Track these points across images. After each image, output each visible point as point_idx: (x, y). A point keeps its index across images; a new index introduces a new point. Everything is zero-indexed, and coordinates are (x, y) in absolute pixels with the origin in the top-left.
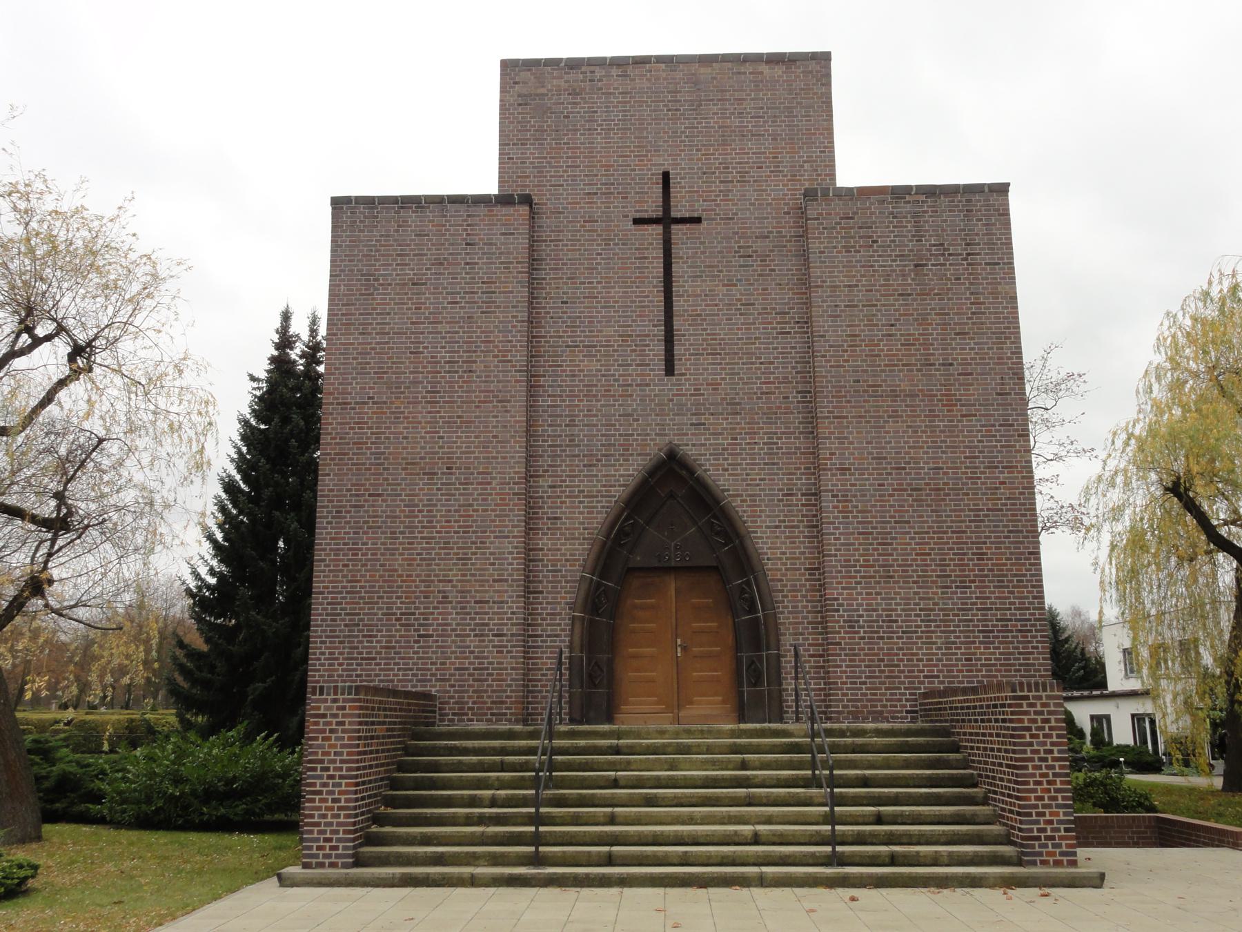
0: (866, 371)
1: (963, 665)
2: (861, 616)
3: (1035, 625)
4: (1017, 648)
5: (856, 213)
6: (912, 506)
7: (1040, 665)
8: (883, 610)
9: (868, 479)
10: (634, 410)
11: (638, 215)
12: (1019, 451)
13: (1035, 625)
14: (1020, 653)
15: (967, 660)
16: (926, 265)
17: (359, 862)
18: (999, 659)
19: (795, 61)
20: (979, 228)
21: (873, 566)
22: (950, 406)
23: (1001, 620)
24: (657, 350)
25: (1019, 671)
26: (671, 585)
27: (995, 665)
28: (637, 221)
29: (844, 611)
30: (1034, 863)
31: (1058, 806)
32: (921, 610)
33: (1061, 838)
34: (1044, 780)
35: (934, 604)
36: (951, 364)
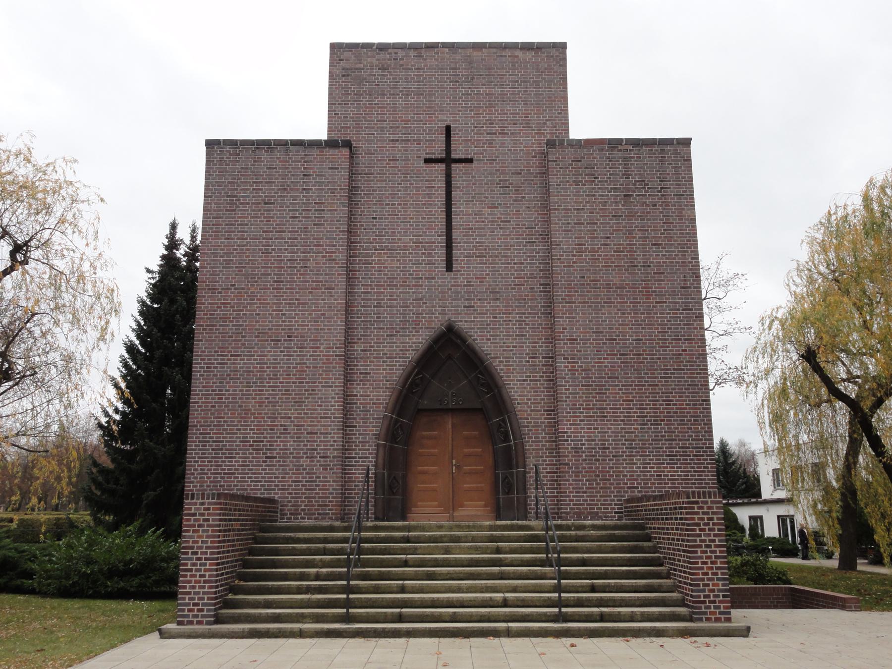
0: (589, 270)
2: (584, 444)
4: (694, 468)
6: (620, 366)
7: (709, 480)
10: (423, 296)
11: (428, 157)
14: (695, 471)
17: (218, 620)
18: (681, 476)
20: (670, 170)
23: (682, 448)
24: (440, 254)
26: (449, 422)
28: (427, 161)
30: (701, 620)
31: (718, 579)
33: (720, 602)
34: (709, 561)
36: (649, 266)
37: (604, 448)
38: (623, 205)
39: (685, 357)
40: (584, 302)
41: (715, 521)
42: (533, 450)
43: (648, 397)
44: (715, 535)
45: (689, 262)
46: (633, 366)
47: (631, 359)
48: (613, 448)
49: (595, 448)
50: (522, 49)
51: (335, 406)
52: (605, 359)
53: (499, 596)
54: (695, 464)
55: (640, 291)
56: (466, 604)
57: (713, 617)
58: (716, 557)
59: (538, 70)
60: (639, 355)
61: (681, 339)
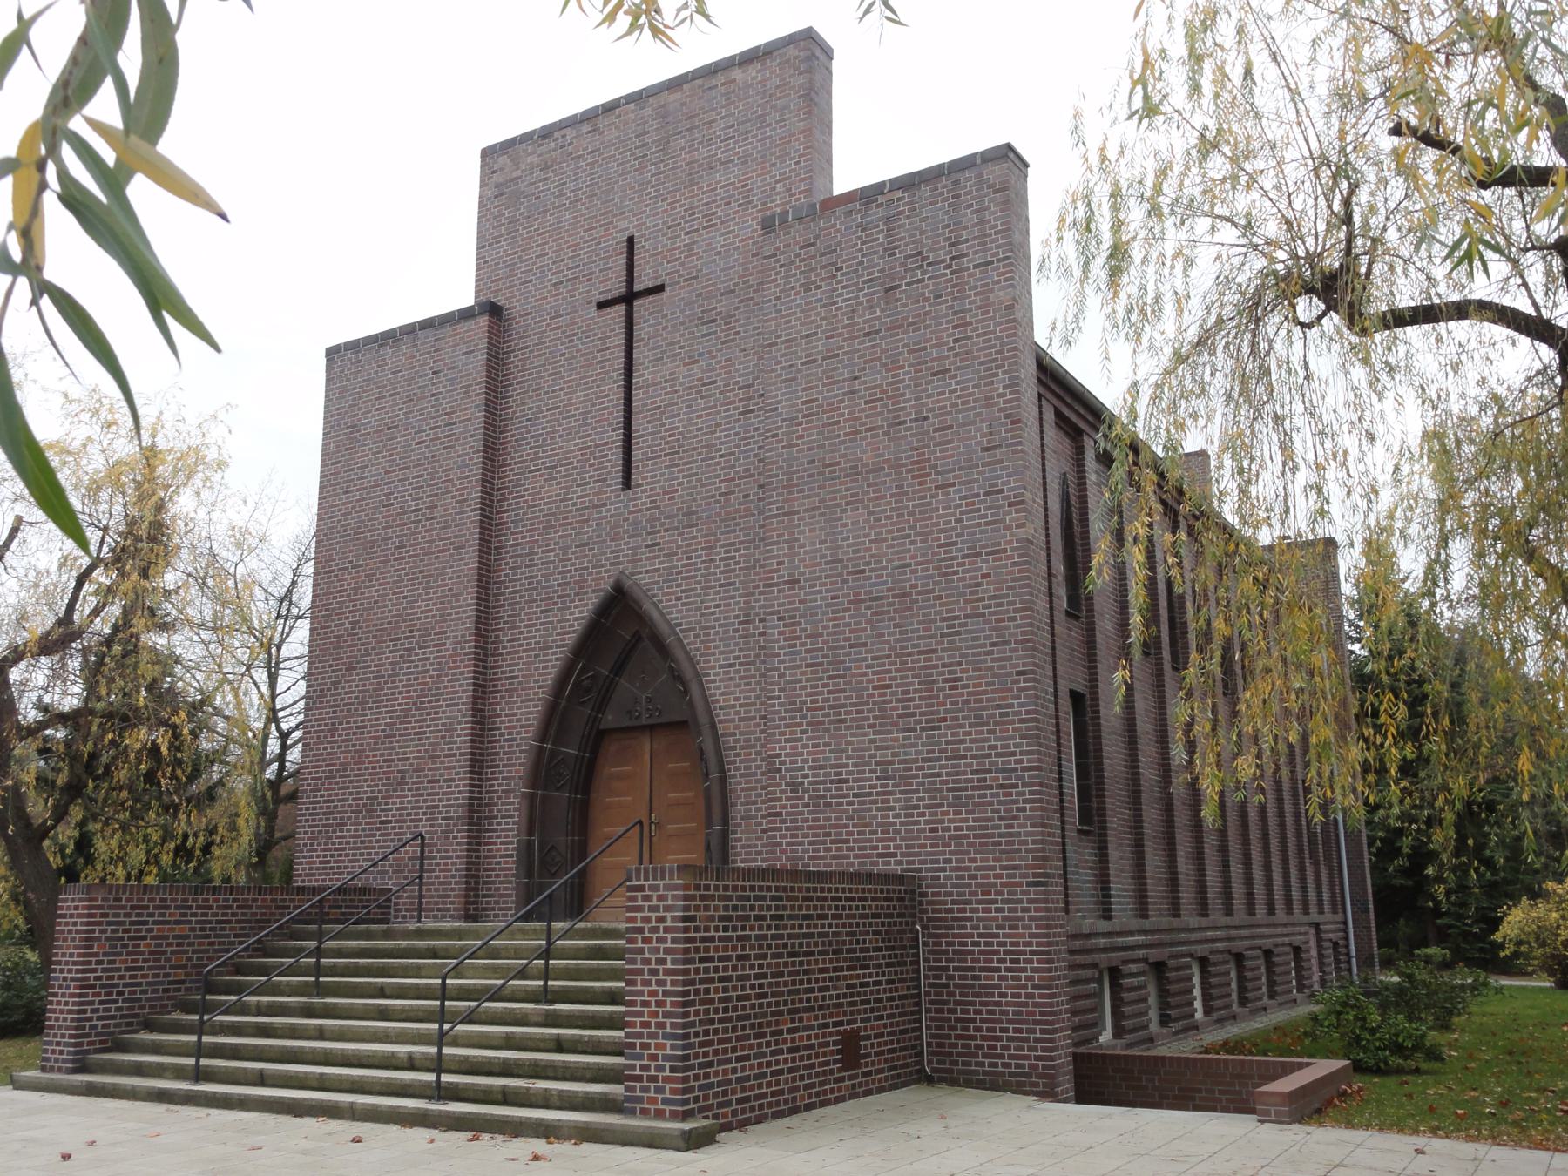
0: (822, 446)
1: (926, 838)
2: (806, 776)
3: (1022, 777)
4: (998, 811)
6: (871, 622)
7: (1027, 834)
8: (832, 767)
9: (820, 592)
10: (590, 538)
11: (602, 298)
12: (1009, 528)
13: (1022, 777)
14: (1001, 819)
15: (931, 830)
16: (899, 286)
17: (83, 1068)
18: (973, 828)
19: (770, 53)
20: (968, 218)
21: (822, 708)
22: (922, 477)
23: (977, 772)
24: (617, 457)
25: (999, 843)
26: (645, 745)
27: (967, 836)
29: (787, 770)
30: (632, 1112)
31: (665, 1036)
32: (877, 763)
33: (666, 1079)
34: (653, 999)
35: (894, 754)
36: (926, 418)
37: (840, 781)
38: (882, 310)
39: (988, 589)
40: (813, 509)
41: (669, 924)
42: (742, 790)
43: (918, 676)
44: (667, 951)
45: (999, 396)
46: (894, 619)
47: (890, 604)
48: (855, 780)
49: (824, 782)
50: (741, 64)
51: (462, 735)
52: (845, 610)
53: (403, 1049)
54: (999, 803)
55: (909, 471)
56: (365, 1062)
57: (653, 1108)
58: (665, 993)
60: (904, 595)
61: (980, 554)
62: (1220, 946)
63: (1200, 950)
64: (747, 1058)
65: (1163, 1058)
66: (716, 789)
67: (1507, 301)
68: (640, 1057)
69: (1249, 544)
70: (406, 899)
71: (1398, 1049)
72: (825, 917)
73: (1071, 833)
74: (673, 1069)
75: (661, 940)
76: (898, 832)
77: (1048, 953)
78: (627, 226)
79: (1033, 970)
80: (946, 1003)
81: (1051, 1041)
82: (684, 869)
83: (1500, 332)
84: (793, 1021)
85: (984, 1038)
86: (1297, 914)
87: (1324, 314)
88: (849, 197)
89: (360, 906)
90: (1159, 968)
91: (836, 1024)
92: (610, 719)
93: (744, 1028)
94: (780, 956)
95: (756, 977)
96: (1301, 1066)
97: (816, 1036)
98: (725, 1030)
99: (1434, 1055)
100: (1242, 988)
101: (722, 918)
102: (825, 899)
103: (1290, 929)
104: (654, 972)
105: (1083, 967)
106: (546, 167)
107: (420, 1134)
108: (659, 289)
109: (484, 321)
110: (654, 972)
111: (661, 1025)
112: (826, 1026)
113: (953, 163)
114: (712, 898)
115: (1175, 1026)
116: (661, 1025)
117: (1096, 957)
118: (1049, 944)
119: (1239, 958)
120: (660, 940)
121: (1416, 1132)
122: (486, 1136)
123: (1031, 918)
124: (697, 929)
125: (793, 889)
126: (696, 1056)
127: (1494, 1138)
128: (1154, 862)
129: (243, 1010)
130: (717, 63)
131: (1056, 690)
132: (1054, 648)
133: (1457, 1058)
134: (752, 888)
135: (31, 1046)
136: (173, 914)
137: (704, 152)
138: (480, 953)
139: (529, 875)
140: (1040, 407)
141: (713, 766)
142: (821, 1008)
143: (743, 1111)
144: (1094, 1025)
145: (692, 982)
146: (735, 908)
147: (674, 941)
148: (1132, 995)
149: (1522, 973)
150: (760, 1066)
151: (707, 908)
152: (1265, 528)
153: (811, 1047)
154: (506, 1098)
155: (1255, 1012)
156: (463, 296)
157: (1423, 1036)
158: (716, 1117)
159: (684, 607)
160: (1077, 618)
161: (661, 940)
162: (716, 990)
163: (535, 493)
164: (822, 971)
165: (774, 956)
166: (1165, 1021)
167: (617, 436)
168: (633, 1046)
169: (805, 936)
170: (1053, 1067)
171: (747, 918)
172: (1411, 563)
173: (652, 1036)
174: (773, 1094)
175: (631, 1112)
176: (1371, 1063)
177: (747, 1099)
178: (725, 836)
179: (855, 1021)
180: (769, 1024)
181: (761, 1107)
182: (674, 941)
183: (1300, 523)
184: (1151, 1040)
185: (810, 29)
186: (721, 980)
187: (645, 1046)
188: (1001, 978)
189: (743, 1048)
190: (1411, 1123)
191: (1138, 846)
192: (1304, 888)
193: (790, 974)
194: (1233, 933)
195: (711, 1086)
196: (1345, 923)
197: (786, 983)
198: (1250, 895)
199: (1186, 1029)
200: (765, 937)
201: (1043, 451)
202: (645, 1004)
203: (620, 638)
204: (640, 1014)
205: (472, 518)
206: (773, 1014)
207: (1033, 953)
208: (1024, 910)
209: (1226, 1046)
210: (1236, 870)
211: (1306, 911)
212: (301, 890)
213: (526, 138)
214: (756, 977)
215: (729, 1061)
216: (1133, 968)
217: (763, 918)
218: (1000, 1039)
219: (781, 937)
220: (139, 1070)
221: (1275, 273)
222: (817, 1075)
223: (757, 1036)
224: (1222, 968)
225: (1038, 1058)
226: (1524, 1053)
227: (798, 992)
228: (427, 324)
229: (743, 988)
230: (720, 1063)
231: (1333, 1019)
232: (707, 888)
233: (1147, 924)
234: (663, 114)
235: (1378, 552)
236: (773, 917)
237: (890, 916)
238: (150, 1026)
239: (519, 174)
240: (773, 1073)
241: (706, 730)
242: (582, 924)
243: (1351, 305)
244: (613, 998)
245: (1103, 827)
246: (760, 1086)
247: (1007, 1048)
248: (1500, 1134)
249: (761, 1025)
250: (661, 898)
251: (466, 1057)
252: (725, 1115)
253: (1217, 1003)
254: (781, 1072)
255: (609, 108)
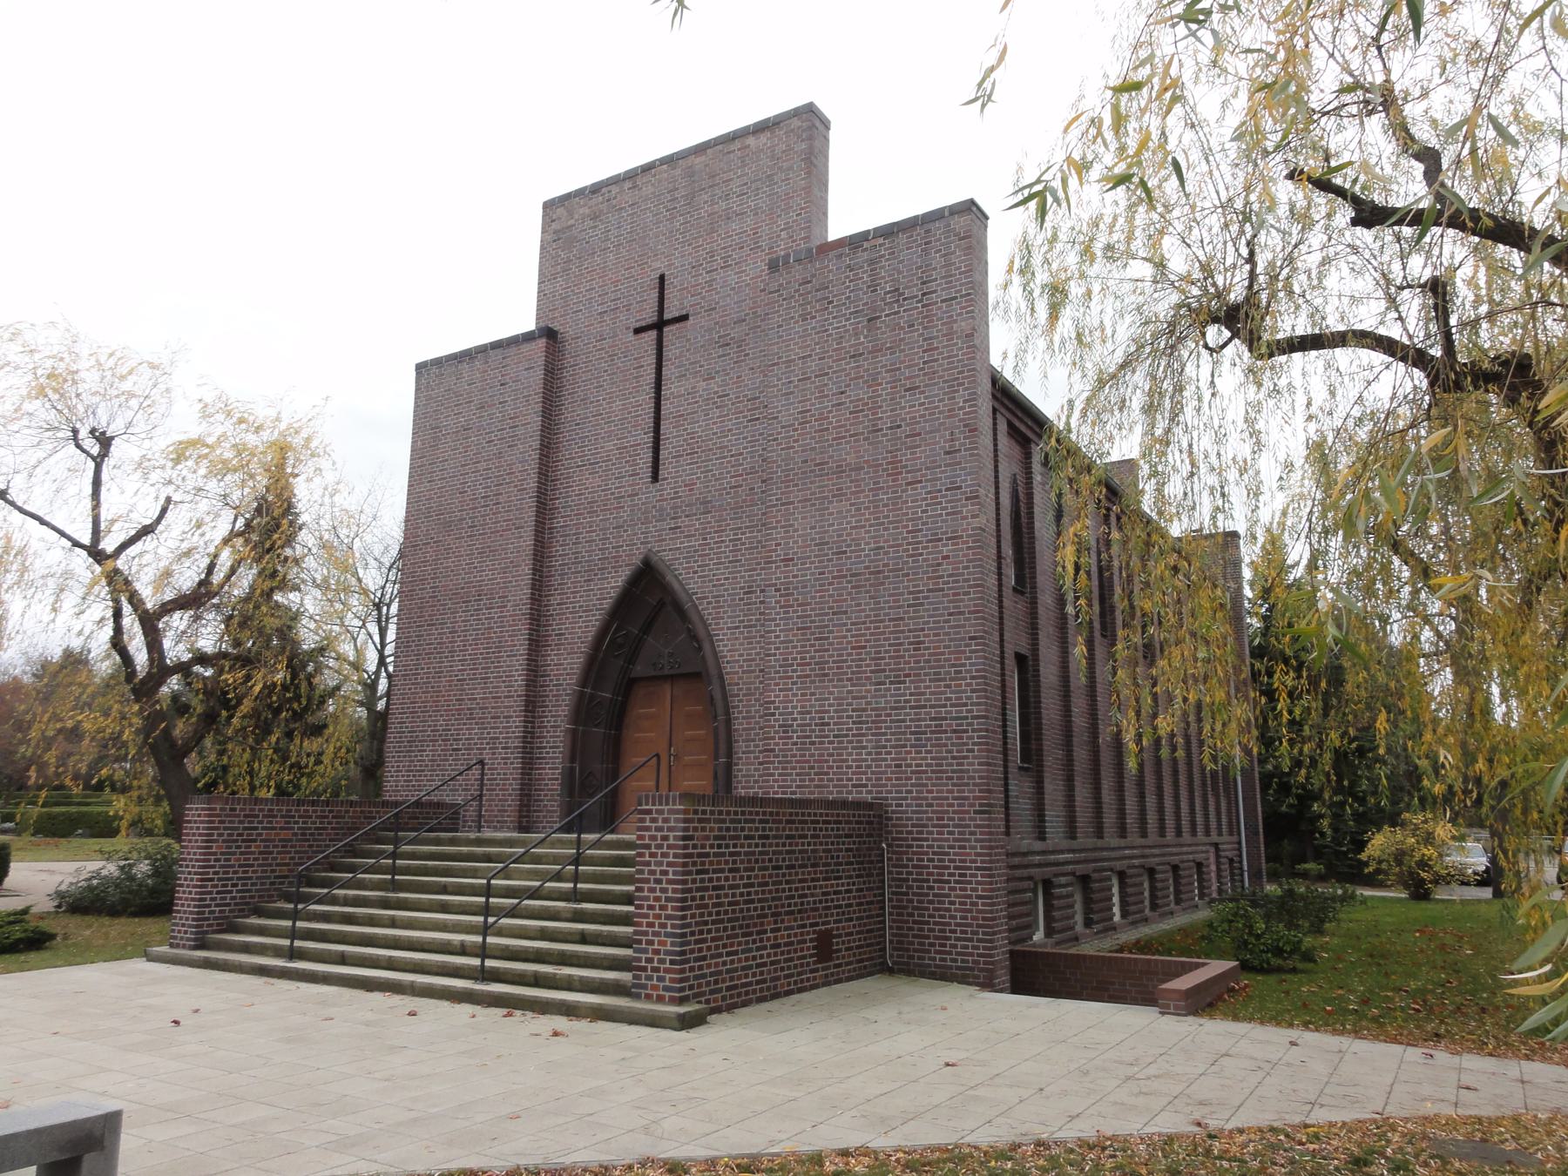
5: (813, 276)
7: (975, 771)
11: (638, 325)
14: (954, 758)
20: (937, 260)
24: (646, 456)
26: (667, 690)
31: (667, 935)
33: (667, 971)
35: (868, 703)
39: (947, 568)
44: (669, 864)
51: (519, 681)
53: (456, 938)
58: (667, 899)
59: (772, 157)
62: (1136, 862)
63: (1118, 865)
64: (736, 953)
65: (1084, 956)
66: (722, 730)
67: (1382, 331)
68: (645, 951)
69: (1164, 535)
70: (471, 812)
71: (1278, 952)
72: (805, 837)
73: (1013, 770)
74: (672, 962)
75: (664, 855)
76: (869, 767)
77: (990, 869)
78: (659, 266)
79: (978, 883)
80: (905, 908)
81: (991, 941)
82: (686, 796)
83: (1378, 358)
84: (776, 922)
85: (936, 938)
86: (1201, 837)
87: (1230, 340)
88: (840, 243)
89: (434, 817)
90: (1084, 880)
91: (812, 925)
92: (639, 670)
93: (733, 928)
94: (766, 869)
95: (745, 886)
96: (1198, 966)
97: (796, 935)
98: (718, 930)
99: (1308, 957)
100: (1153, 896)
101: (716, 838)
102: (805, 822)
103: (1195, 848)
104: (658, 881)
105: (1021, 879)
106: (595, 217)
107: (467, 1009)
108: (684, 318)
109: (542, 342)
110: (658, 881)
111: (663, 926)
112: (804, 926)
113: (925, 216)
114: (708, 820)
115: (1096, 927)
116: (663, 926)
117: (1033, 871)
118: (991, 862)
119: (1151, 872)
120: (663, 855)
121: (1291, 1025)
122: (518, 1013)
123: (977, 840)
124: (695, 847)
125: (778, 814)
126: (692, 951)
127: (1356, 1032)
128: (1082, 793)
129: (334, 901)
130: (735, 132)
131: (1002, 652)
132: (1001, 618)
133: (1328, 959)
134: (743, 813)
135: (151, 925)
136: (279, 822)
137: (723, 205)
138: (526, 858)
139: (571, 794)
140: (995, 419)
141: (720, 710)
142: (800, 912)
143: (732, 997)
144: (1028, 926)
145: (689, 890)
146: (728, 829)
147: (675, 856)
148: (1062, 902)
149: (1381, 885)
150: (747, 959)
151: (703, 829)
152: (1176, 522)
153: (791, 943)
154: (537, 981)
155: (1163, 915)
156: (526, 321)
157: (1300, 942)
158: (707, 1002)
159: (700, 578)
160: (1022, 593)
161: (664, 855)
162: (710, 897)
163: (581, 484)
164: (800, 881)
165: (760, 869)
166: (1088, 923)
167: (648, 438)
168: (640, 942)
169: (788, 852)
170: (992, 963)
171: (738, 837)
172: (1298, 553)
173: (655, 934)
174: (758, 982)
175: (637, 997)
176: (1256, 963)
177: (735, 987)
178: (729, 767)
179: (828, 923)
180: (755, 925)
181: (747, 993)
182: (675, 856)
183: (1203, 517)
184: (1077, 939)
185: (811, 104)
186: (714, 888)
187: (650, 943)
188: (951, 889)
189: (732, 945)
190: (1287, 1017)
191: (1070, 780)
192: (1206, 816)
193: (774, 883)
194: (1147, 851)
195: (704, 976)
196: (1240, 843)
197: (770, 892)
198: (1162, 820)
199: (1106, 930)
200: (753, 853)
201: (996, 456)
202: (651, 907)
203: (648, 602)
204: (646, 916)
205: (529, 506)
206: (759, 916)
207: (977, 869)
208: (972, 833)
209: (1142, 946)
210: (1151, 801)
211: (1207, 833)
212: (385, 804)
213: (580, 193)
214: (745, 886)
215: (720, 955)
216: (1063, 880)
217: (752, 837)
218: (949, 938)
219: (767, 853)
220: (246, 949)
221: (1188, 306)
222: (796, 966)
223: (744, 935)
224: (1138, 880)
225: (979, 955)
226: (1383, 956)
227: (780, 899)
228: (497, 345)
229: (734, 895)
230: (712, 957)
231: (1226, 926)
232: (704, 812)
233: (1075, 844)
234: (690, 173)
235: (1274, 547)
236: (760, 837)
237: (860, 836)
238: (260, 913)
239: (574, 224)
240: (758, 966)
241: (715, 681)
242: (609, 837)
243: (1251, 332)
244: (628, 899)
245: (1040, 765)
246: (746, 976)
247: (955, 946)
248: (1362, 1028)
249: (748, 926)
250: (666, 820)
251: (507, 947)
252: (715, 1000)
253: (1133, 908)
254: (764, 964)
255: (647, 168)
